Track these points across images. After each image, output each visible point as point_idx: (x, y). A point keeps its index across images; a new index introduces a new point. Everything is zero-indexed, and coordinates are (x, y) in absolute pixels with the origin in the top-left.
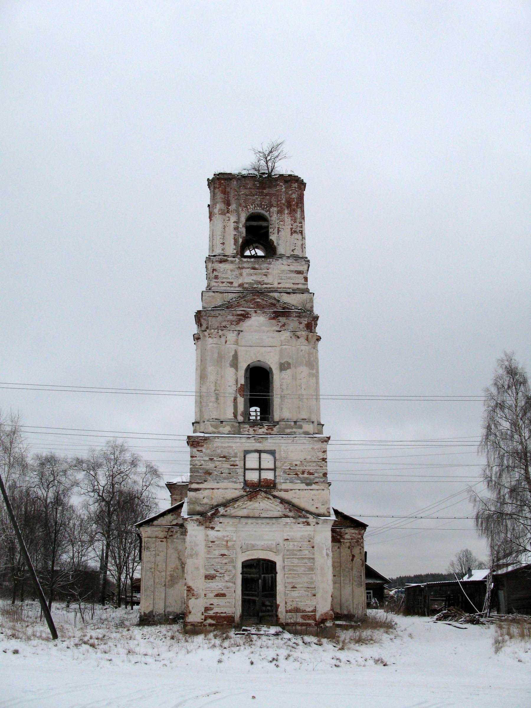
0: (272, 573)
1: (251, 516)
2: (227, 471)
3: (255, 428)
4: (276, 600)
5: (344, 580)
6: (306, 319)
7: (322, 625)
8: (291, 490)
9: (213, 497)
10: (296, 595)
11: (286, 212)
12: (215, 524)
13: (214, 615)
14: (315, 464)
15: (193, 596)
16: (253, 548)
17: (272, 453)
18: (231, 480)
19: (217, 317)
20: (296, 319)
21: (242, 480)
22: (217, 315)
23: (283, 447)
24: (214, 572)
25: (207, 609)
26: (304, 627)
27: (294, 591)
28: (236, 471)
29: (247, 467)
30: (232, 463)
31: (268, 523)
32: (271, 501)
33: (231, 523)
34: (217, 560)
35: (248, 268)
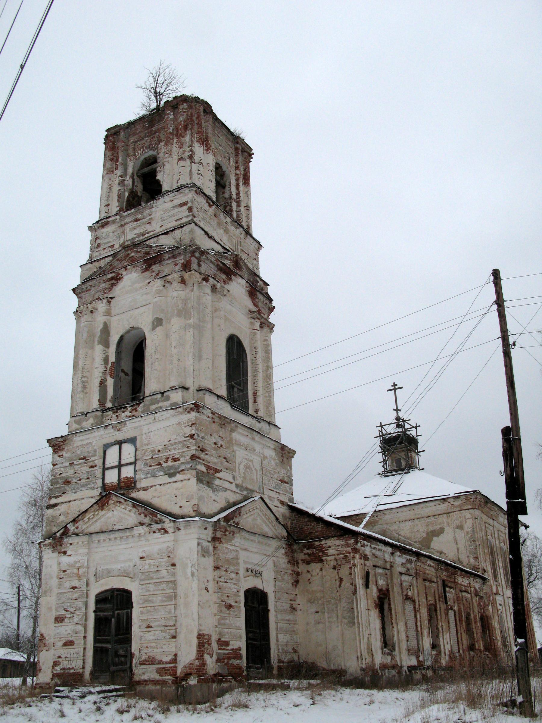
0: (128, 608)
1: (104, 530)
2: (85, 476)
3: (118, 414)
4: (131, 647)
5: (328, 618)
6: (182, 257)
7: (184, 683)
8: (152, 487)
9: (69, 512)
10: (152, 638)
11: (175, 141)
12: (66, 547)
13: (62, 671)
14: (180, 446)
15: (45, 646)
16: (109, 573)
17: (132, 441)
18: (89, 486)
19: (90, 290)
20: (170, 262)
21: (100, 483)
22: (89, 287)
23: (145, 430)
24: (63, 612)
25: (56, 664)
26: (158, 687)
27: (149, 631)
28: (94, 474)
29: (107, 466)
30: (91, 464)
31: (121, 538)
32: (123, 507)
33: (80, 543)
34: (67, 595)
35: (130, 222)
